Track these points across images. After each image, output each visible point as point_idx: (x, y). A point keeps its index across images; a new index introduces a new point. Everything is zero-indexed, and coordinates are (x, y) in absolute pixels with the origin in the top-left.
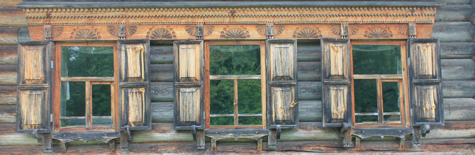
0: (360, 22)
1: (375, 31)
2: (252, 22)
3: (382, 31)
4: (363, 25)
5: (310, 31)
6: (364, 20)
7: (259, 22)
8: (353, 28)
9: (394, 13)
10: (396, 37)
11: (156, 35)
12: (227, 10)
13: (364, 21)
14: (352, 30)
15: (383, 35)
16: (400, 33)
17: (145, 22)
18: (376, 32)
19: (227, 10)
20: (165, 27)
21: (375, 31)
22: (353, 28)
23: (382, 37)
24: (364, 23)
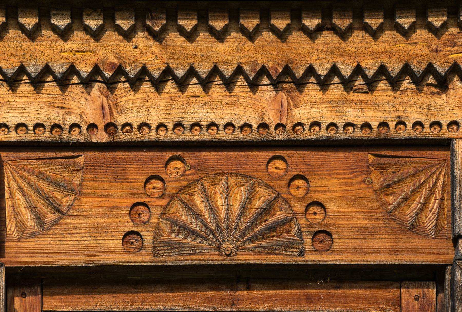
0: (92, 127)
1: (208, 199)
2: (144, 125)
3: (258, 204)
4: (120, 155)
5: (250, 197)
6: (122, 111)
7: (278, 126)
8: (41, 175)
9: (343, 54)
10: (357, 251)
11: (272, 247)
12: (445, 26)
13: (121, 120)
14: (38, 191)
15: (263, 235)
16: (390, 214)
17: (227, 119)
18: (213, 211)
19: (445, 26)
20: (315, 182)
21: (208, 199)
22: (41, 175)
23: (252, 251)
24: (122, 137)
